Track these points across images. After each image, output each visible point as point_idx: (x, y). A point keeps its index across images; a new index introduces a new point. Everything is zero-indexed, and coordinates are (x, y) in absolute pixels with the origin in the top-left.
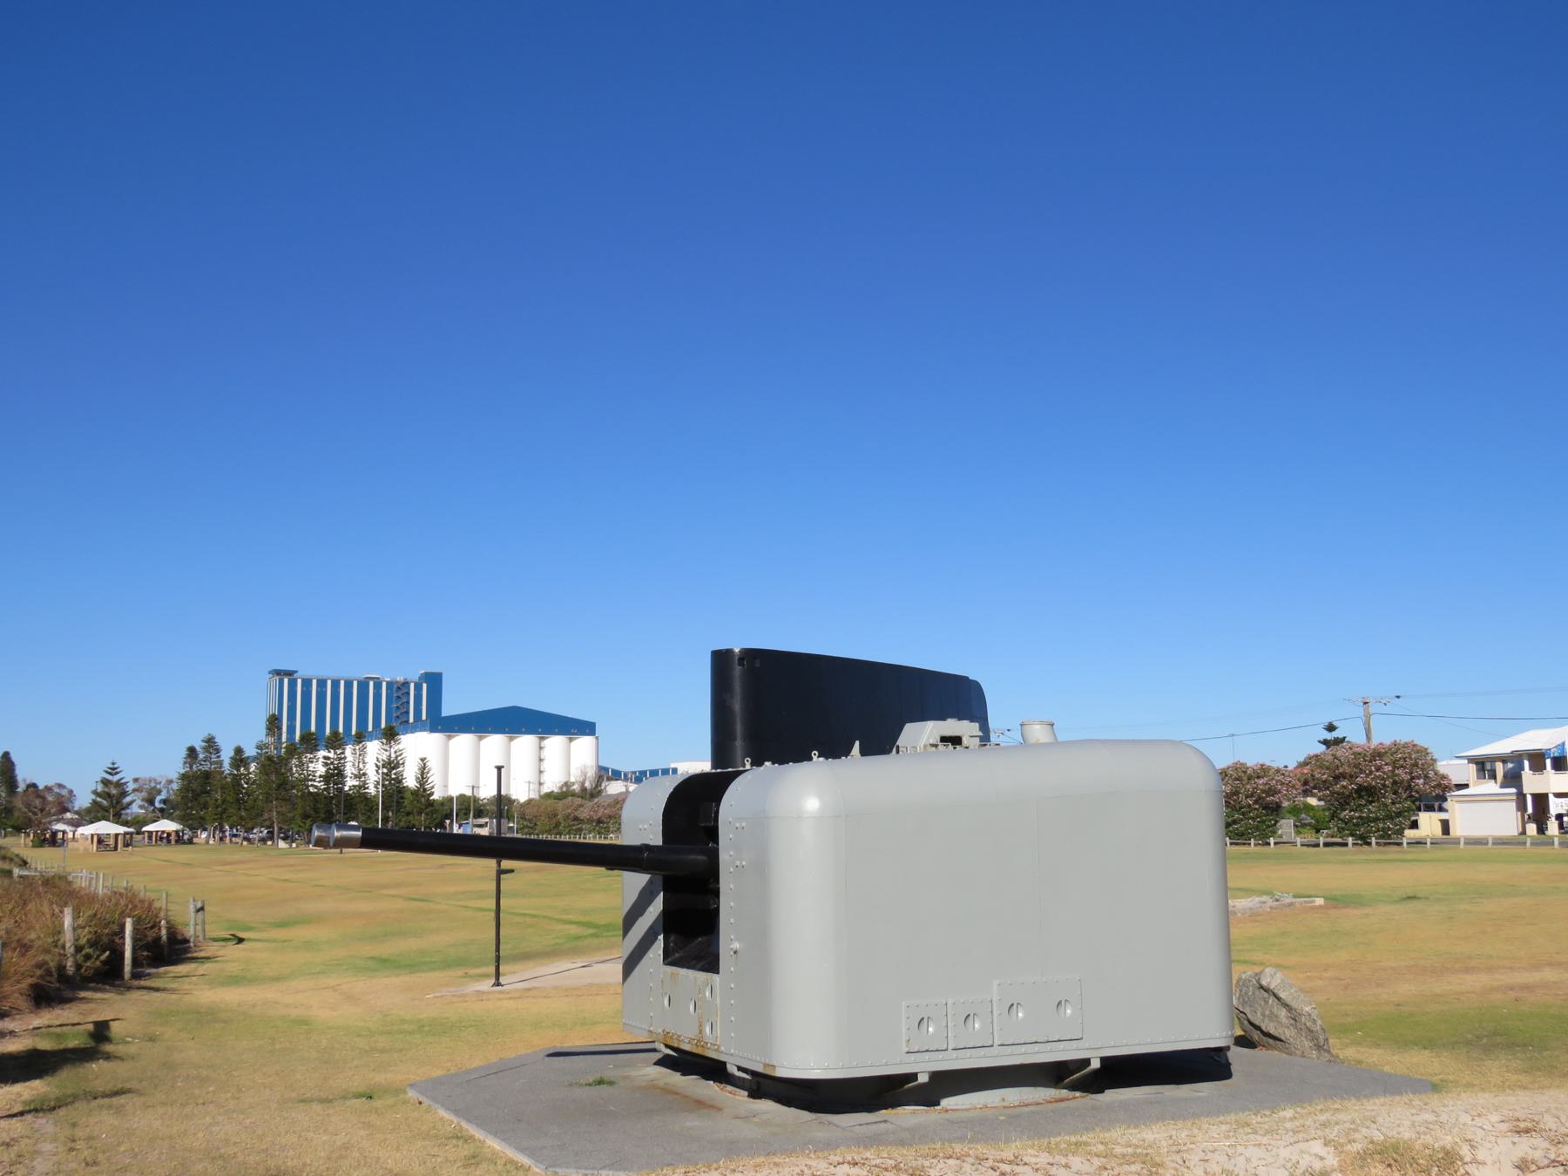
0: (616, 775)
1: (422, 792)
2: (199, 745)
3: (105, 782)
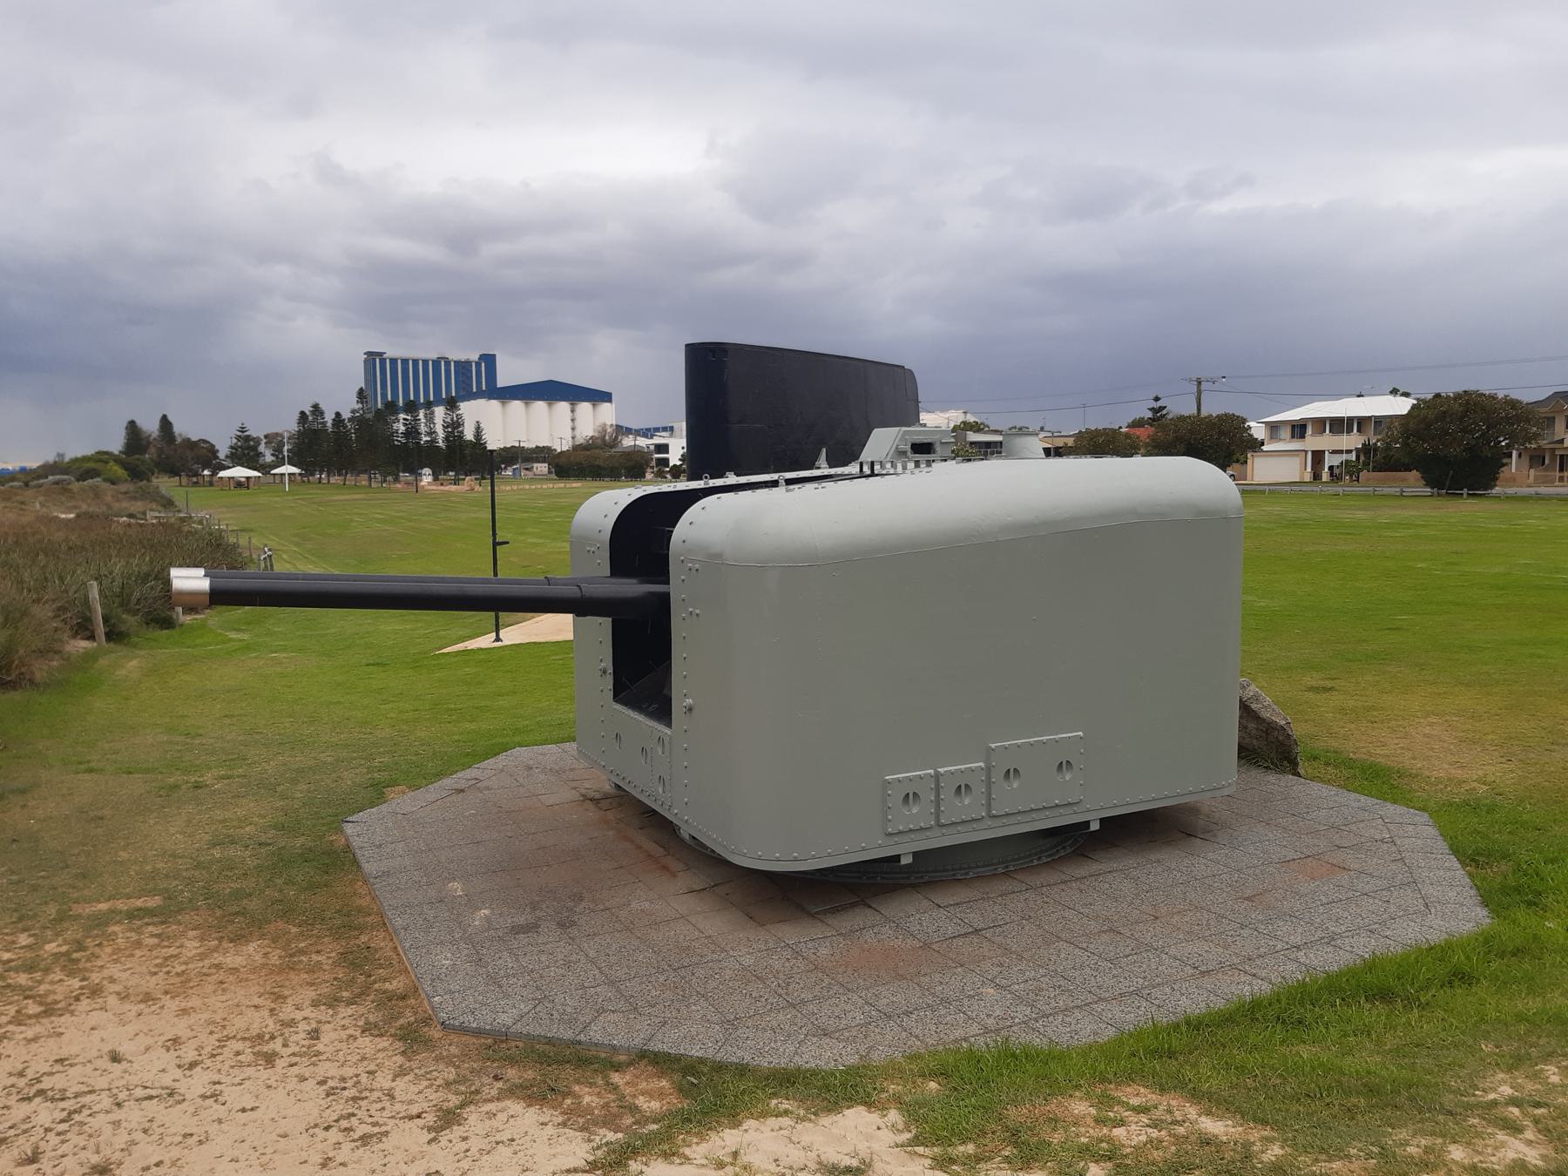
0: (629, 431)
1: (479, 443)
2: (308, 409)
3: (238, 438)
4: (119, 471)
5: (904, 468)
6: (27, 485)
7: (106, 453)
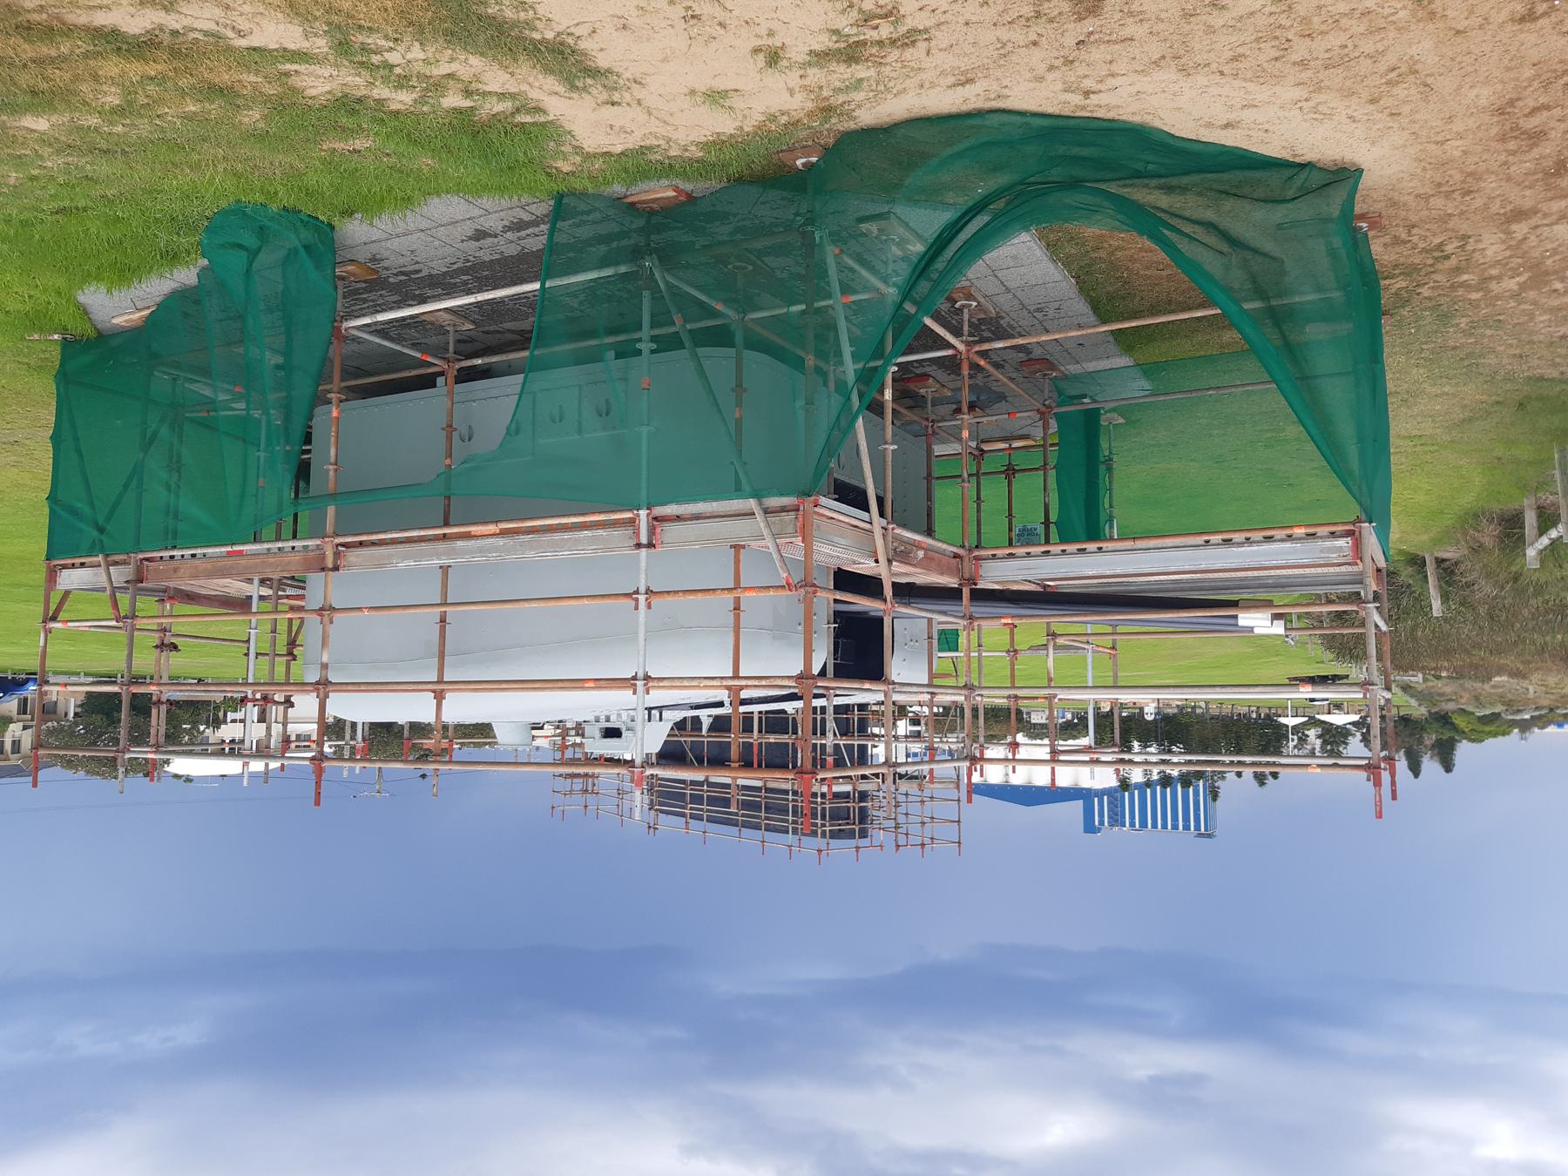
4: (1459, 721)
5: (619, 715)
6: (1551, 710)
7: (1473, 741)
